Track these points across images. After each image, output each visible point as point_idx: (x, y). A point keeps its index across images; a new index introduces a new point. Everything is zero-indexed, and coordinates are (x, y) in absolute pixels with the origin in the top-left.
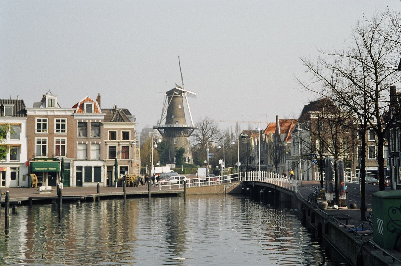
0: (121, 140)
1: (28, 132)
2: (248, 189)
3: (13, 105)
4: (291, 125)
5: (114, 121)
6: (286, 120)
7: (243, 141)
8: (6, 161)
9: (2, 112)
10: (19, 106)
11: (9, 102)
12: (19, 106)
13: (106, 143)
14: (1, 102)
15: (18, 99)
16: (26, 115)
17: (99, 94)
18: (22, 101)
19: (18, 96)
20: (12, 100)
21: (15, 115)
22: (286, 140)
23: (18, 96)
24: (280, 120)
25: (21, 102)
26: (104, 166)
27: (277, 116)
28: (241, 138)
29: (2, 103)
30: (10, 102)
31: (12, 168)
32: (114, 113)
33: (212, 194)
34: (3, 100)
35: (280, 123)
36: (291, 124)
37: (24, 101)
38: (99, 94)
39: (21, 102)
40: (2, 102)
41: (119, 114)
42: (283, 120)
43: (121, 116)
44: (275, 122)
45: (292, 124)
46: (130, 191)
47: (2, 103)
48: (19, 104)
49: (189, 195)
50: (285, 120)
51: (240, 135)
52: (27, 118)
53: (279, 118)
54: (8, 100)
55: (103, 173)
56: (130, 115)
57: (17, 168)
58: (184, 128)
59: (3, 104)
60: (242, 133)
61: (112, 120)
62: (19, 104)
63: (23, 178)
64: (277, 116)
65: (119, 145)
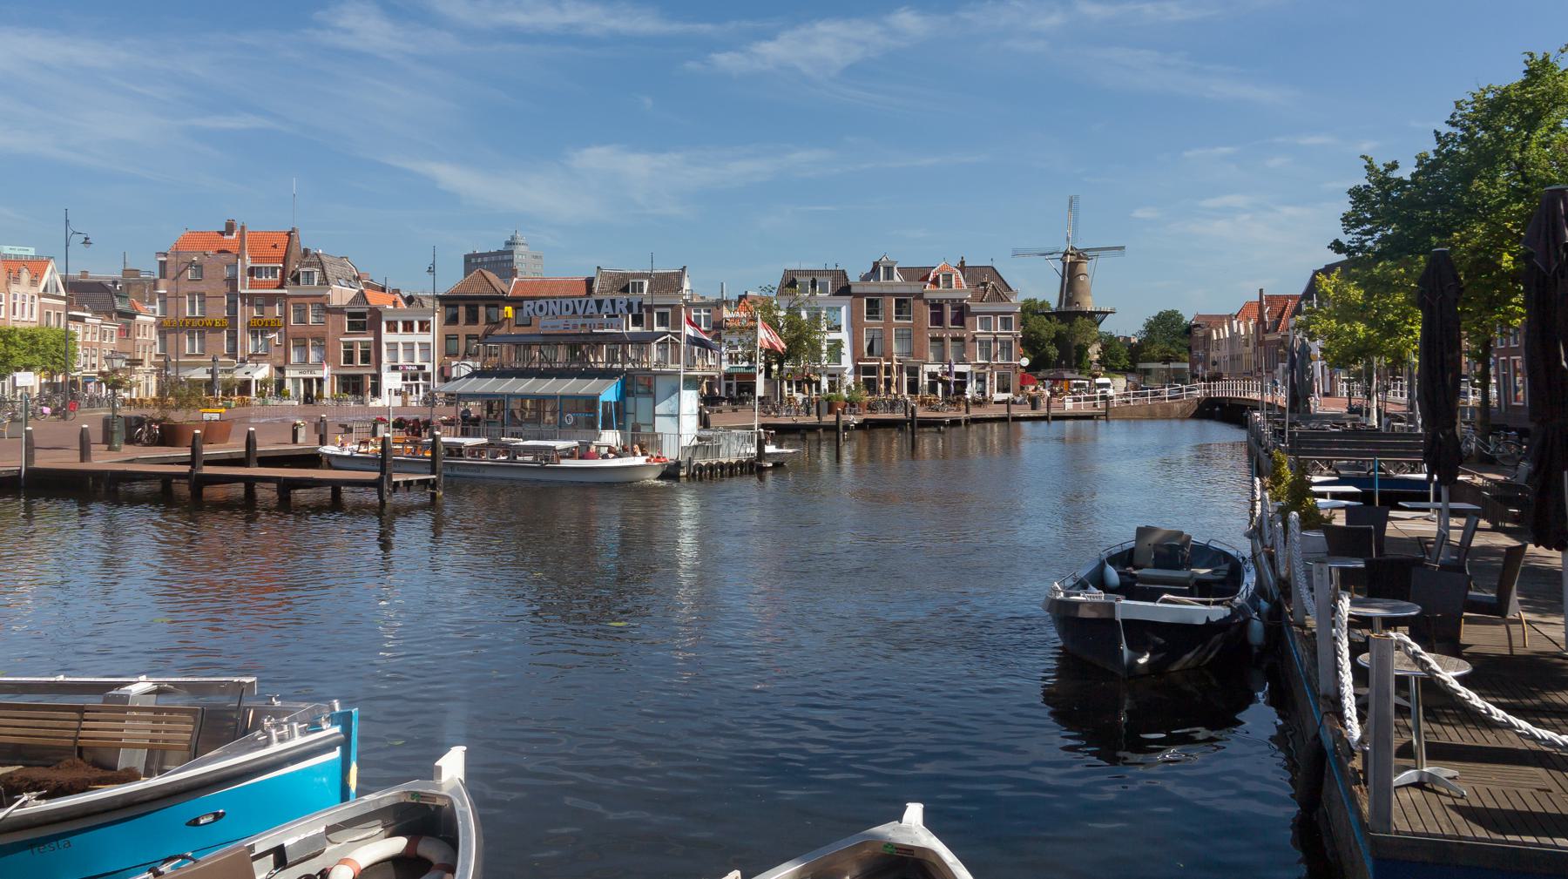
42: (1271, 296)
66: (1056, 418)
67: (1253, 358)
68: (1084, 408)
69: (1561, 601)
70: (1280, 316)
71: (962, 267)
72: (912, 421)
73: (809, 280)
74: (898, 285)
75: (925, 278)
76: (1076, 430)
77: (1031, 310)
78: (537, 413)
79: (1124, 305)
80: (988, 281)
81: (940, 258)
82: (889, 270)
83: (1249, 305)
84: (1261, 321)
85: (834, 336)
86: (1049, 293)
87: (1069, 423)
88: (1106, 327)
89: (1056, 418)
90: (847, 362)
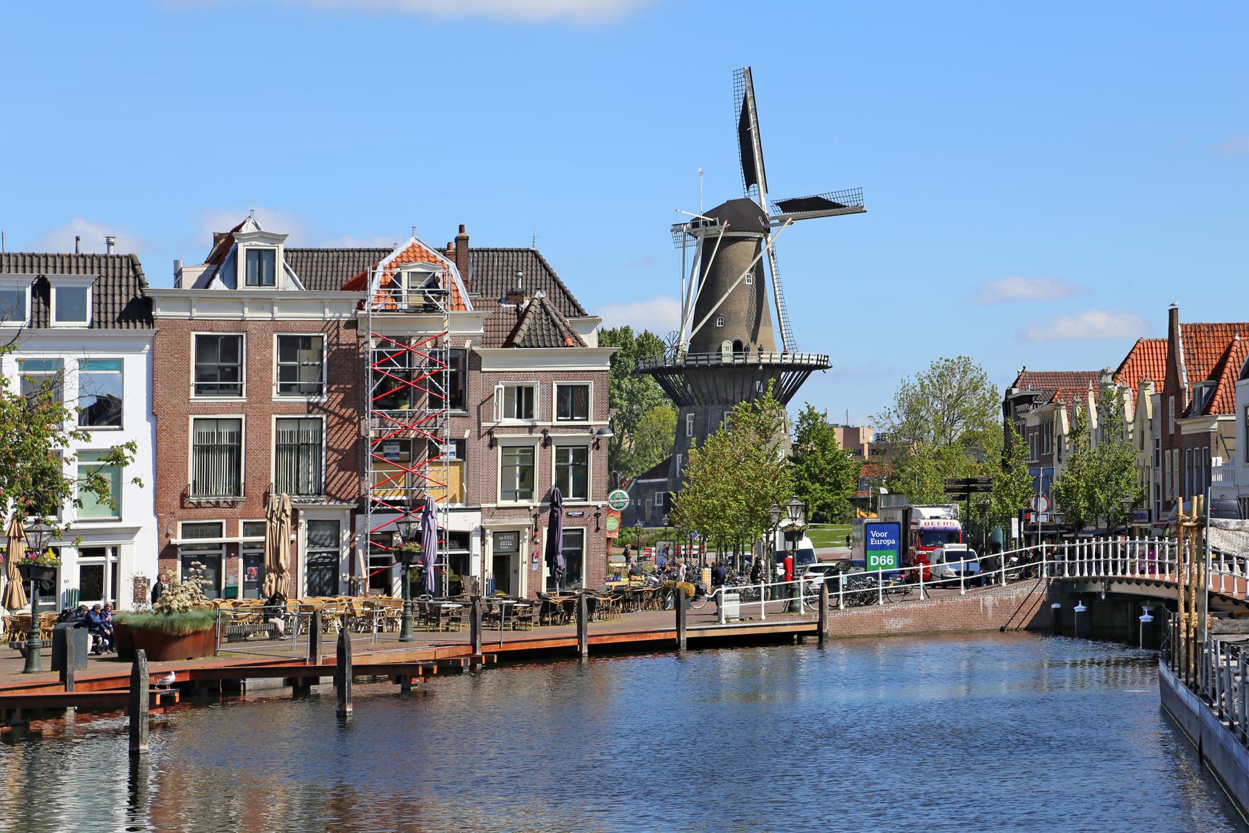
0: (555, 423)
1: (160, 392)
2: (1080, 608)
3: (91, 277)
4: (1234, 349)
5: (528, 343)
6: (1211, 327)
7: (1022, 416)
8: (120, 520)
9: (42, 306)
10: (117, 283)
11: (74, 264)
12: (117, 283)
13: (544, 432)
14: (5, 263)
15: (112, 253)
16: (150, 321)
17: (461, 228)
18: (132, 262)
19: (108, 238)
20: (82, 256)
21: (99, 322)
22: (1213, 409)
23: (108, 238)
24: (1185, 327)
25: (124, 265)
26: (483, 530)
27: (1173, 313)
28: (1012, 403)
29: (43, 270)
30: (62, 267)
31: (86, 552)
32: (517, 310)
33: (988, 631)
34: (46, 256)
35: (1187, 340)
36: (1231, 345)
37: (140, 259)
38: (461, 228)
39: (124, 265)
40: (39, 266)
41: (547, 314)
42: (1196, 328)
43: (553, 321)
44: (1166, 337)
45: (1236, 343)
46: (603, 627)
47: (43, 270)
48: (117, 274)
49: (839, 638)
50: (1208, 326)
51: (1008, 392)
52: (152, 332)
53: (1183, 319)
54: (70, 256)
55: (479, 559)
56: (580, 312)
57: (109, 552)
58: (765, 365)
59: (43, 272)
60: (1014, 386)
61: (517, 340)
62: (117, 274)
63: (135, 595)
64: (1173, 313)
65: (547, 442)
66: (697, 644)
67: (1154, 477)
68: (768, 616)
69: (234, 374)
70: (1216, 374)
71: (459, 250)
72: (338, 670)
73: (32, 277)
74: (287, 300)
75: (360, 284)
76: (748, 673)
77: (632, 353)
78: (1216, 647)
79: (865, 339)
80: (524, 292)
81: (401, 220)
82: (262, 261)
83: (1141, 348)
84: (1171, 386)
85: (103, 438)
86: (666, 316)
87: (729, 657)
88: (811, 395)
89: (697, 644)
90: (138, 504)
